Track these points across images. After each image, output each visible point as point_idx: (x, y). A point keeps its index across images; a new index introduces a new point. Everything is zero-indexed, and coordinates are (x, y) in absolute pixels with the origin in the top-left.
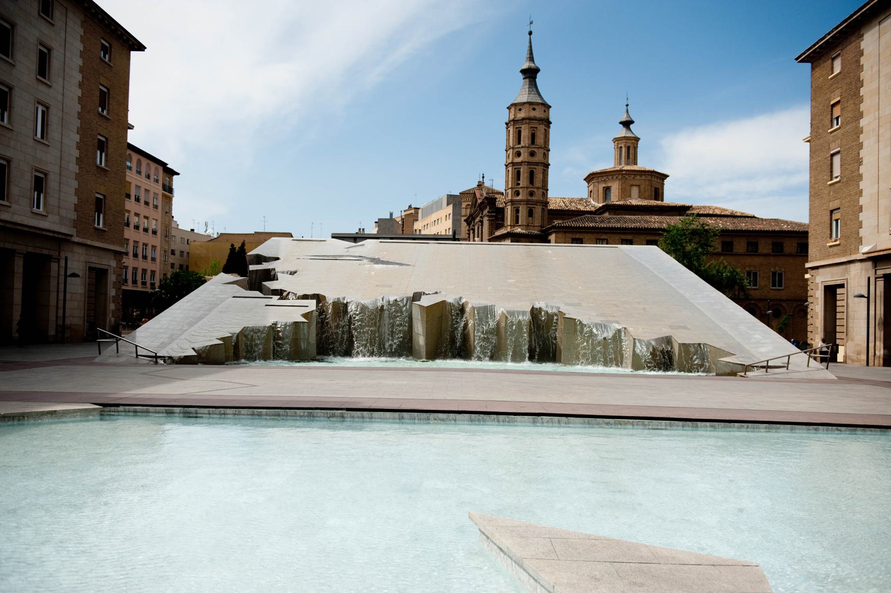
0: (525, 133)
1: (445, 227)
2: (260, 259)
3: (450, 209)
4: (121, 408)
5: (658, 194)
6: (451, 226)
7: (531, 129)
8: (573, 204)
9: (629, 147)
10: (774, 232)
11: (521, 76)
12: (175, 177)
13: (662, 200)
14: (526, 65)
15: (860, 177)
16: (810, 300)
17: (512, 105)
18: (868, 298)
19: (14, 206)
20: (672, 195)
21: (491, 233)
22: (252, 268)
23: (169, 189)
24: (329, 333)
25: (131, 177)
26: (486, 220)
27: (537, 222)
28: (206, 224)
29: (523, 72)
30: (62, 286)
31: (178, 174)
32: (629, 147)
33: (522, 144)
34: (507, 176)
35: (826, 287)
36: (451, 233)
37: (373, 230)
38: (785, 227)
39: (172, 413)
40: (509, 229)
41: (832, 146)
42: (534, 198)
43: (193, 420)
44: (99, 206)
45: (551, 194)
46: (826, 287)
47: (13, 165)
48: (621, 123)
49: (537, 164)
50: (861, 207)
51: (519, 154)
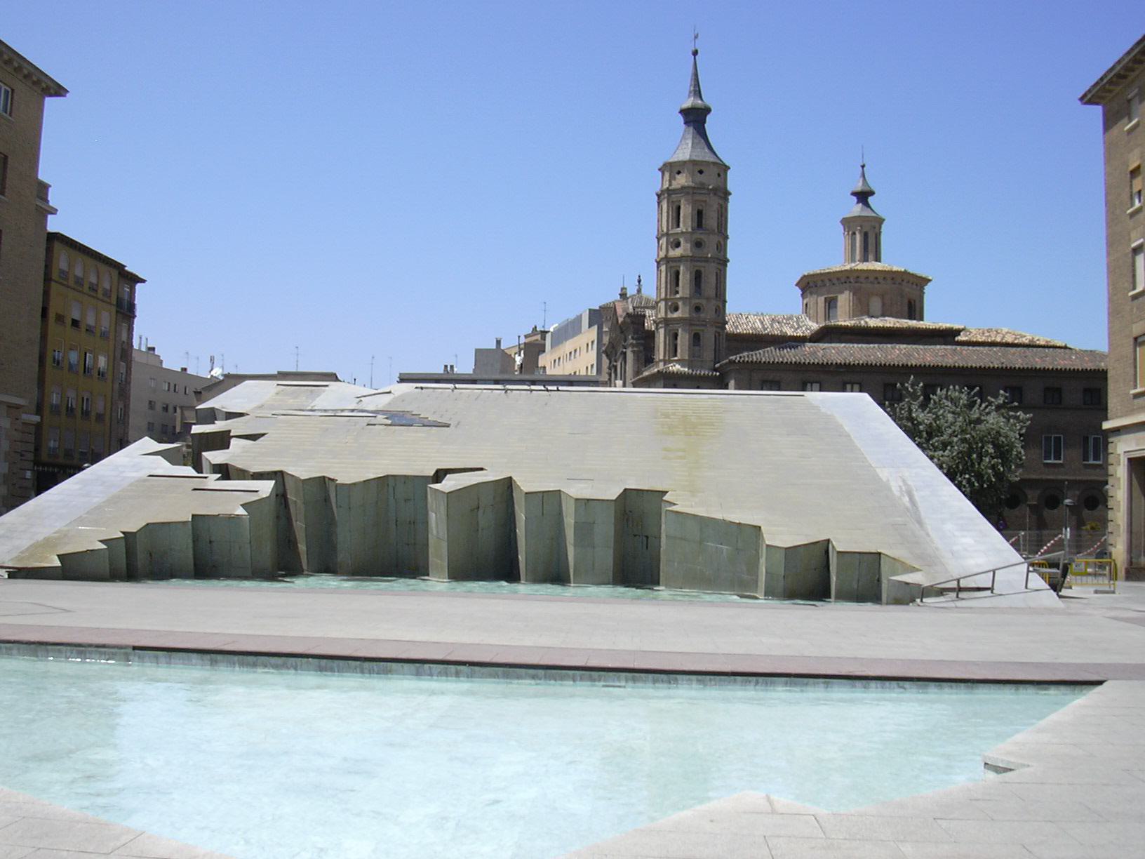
0: (686, 211)
2: (211, 416)
3: (592, 334)
5: (914, 310)
7: (698, 207)
10: (1085, 372)
11: (681, 119)
14: (688, 103)
16: (1111, 481)
17: (665, 165)
20: (932, 319)
21: (637, 373)
24: (312, 533)
27: (709, 355)
28: (212, 360)
29: (685, 113)
32: (867, 234)
33: (682, 228)
34: (659, 279)
37: (466, 366)
40: (661, 366)
41: (1133, 235)
45: (731, 309)
46: (1130, 460)
48: (854, 194)
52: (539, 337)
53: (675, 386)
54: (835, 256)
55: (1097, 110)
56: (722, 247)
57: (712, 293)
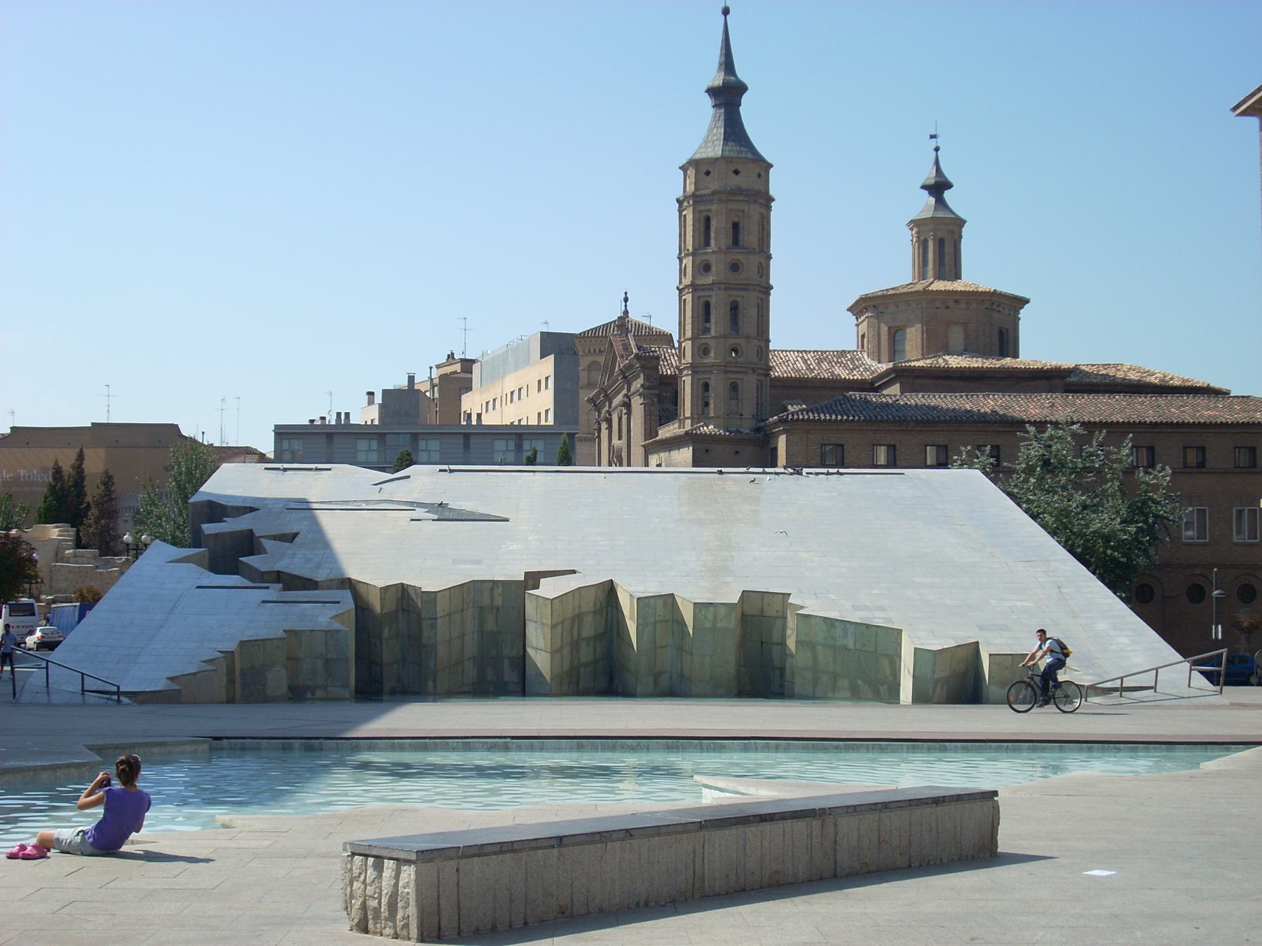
3: (547, 366)
5: (1007, 343)
6: (551, 406)
7: (729, 209)
8: (825, 365)
9: (940, 239)
11: (708, 102)
13: (1016, 356)
20: (1038, 346)
21: (650, 432)
22: (209, 528)
26: (637, 402)
29: (712, 92)
32: (940, 239)
42: (453, 863)
43: (317, 754)
48: (924, 187)
49: (745, 287)
51: (707, 268)
52: (457, 367)
54: (896, 269)
55: (1254, 121)
56: (764, 271)
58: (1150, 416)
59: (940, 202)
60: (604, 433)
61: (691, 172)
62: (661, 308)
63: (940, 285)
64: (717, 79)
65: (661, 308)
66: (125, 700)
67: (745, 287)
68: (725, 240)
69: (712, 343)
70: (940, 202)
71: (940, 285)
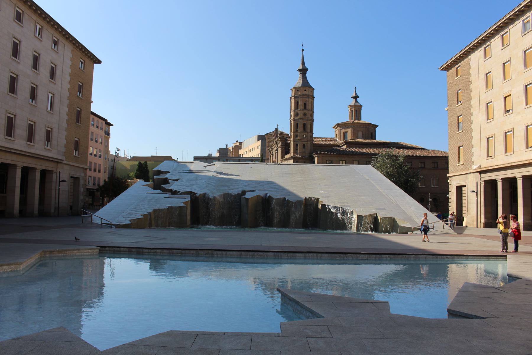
1: (256, 153)
2: (159, 173)
4: (107, 249)
5: (373, 136)
7: (303, 100)
9: (357, 110)
11: (299, 72)
12: (111, 127)
15: (472, 130)
16: (450, 193)
18: (477, 192)
19: (36, 145)
20: (380, 137)
21: (283, 157)
23: (108, 134)
25: (92, 129)
29: (300, 70)
30: (58, 186)
31: (113, 125)
32: (357, 110)
35: (457, 187)
36: (260, 156)
37: (216, 154)
38: (438, 155)
39: (131, 252)
44: (77, 144)
46: (457, 187)
47: (37, 125)
48: (352, 97)
50: (473, 146)
52: (238, 144)
53: (305, 163)
54: (346, 117)
56: (312, 116)
57: (309, 131)
58: (411, 154)
59: (356, 101)
60: (272, 158)
61: (294, 90)
62: (286, 128)
63: (356, 121)
64: (301, 67)
65: (286, 128)
66: (113, 227)
67: (308, 120)
68: (303, 108)
69: (299, 134)
70: (356, 101)
71: (356, 121)
